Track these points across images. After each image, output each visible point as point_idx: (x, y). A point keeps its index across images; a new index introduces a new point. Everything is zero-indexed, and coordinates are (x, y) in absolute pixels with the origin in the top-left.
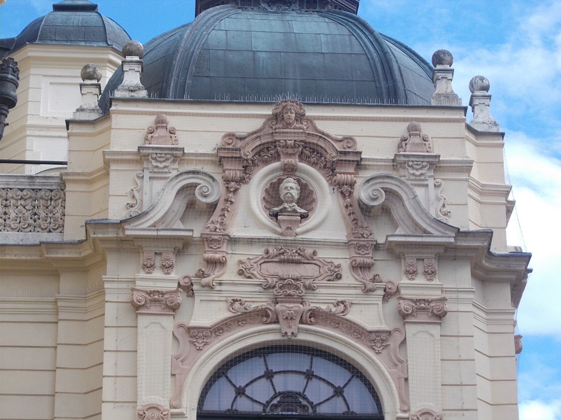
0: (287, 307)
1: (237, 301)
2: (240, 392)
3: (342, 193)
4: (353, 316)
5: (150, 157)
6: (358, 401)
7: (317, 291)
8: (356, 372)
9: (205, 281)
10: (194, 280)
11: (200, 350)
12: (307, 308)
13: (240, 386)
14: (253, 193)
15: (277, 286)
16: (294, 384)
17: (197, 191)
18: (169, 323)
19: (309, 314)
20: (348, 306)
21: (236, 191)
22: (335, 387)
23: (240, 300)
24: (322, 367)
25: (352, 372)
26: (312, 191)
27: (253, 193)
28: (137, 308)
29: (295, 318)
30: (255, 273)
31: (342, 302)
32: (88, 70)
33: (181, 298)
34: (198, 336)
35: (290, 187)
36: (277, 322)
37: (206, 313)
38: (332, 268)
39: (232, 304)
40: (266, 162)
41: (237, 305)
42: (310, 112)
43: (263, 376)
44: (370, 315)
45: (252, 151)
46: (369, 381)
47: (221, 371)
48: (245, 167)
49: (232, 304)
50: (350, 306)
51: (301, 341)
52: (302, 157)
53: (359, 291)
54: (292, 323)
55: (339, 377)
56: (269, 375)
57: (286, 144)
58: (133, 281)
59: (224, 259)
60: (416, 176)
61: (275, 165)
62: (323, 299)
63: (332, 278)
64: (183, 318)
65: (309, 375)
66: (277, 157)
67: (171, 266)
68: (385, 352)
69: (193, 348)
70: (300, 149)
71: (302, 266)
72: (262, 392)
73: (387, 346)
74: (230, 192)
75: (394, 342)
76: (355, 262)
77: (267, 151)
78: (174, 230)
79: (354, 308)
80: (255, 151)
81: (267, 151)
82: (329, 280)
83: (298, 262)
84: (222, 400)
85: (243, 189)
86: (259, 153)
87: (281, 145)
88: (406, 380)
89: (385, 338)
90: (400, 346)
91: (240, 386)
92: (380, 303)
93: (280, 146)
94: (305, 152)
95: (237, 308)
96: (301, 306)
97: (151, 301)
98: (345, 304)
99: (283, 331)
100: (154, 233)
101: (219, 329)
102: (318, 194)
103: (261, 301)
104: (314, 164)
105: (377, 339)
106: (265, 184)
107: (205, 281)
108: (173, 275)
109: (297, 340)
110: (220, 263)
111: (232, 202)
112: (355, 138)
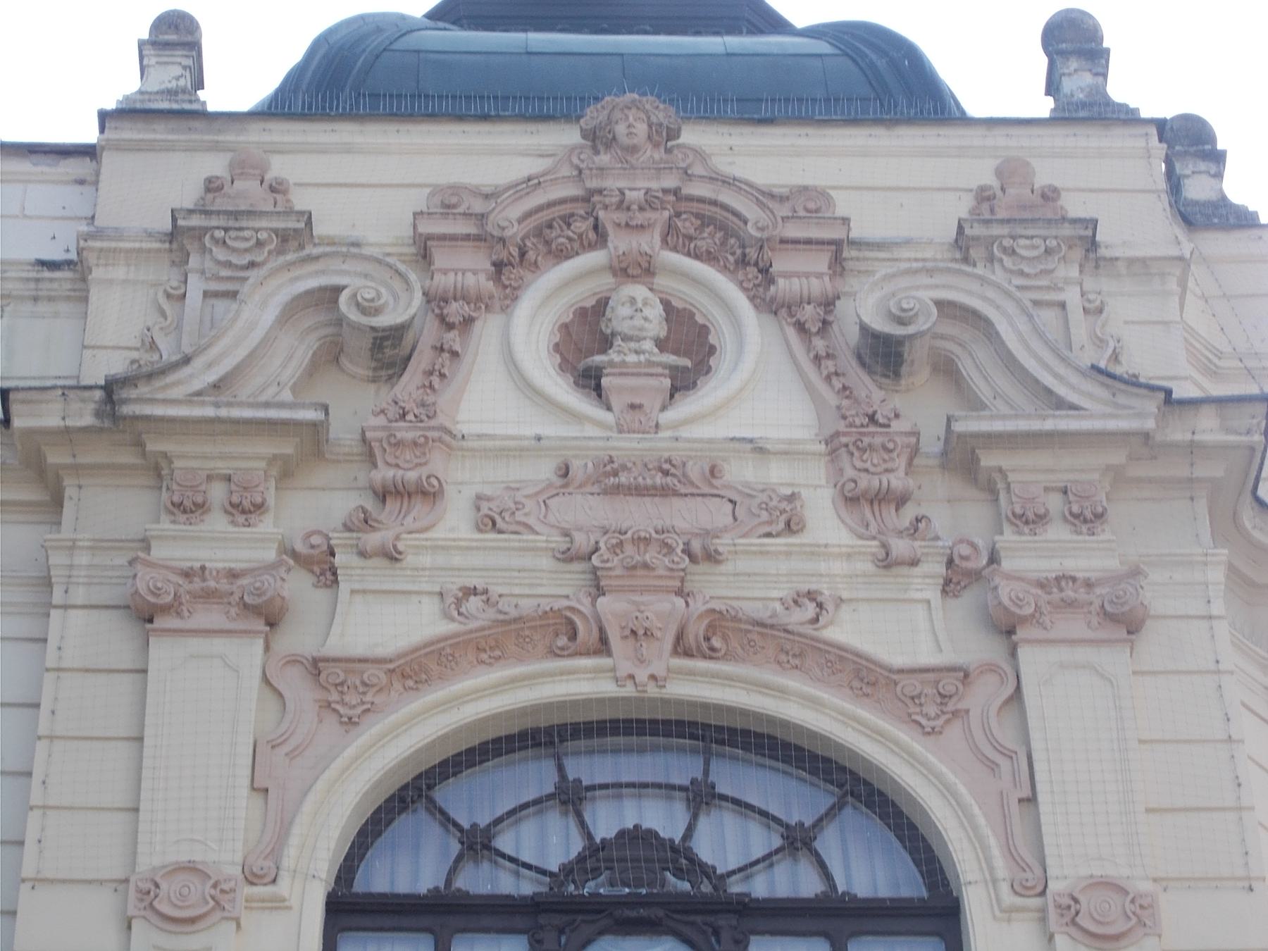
0: (634, 603)
1: (474, 591)
2: (477, 844)
3: (801, 327)
4: (843, 630)
5: (207, 239)
6: (863, 866)
7: (727, 567)
8: (858, 789)
9: (373, 540)
10: (337, 539)
11: (351, 722)
12: (698, 606)
13: (474, 826)
14: (530, 325)
15: (602, 545)
16: (664, 819)
17: (343, 298)
18: (249, 654)
19: (706, 622)
20: (830, 606)
21: (468, 322)
22: (787, 827)
23: (486, 592)
24: (733, 777)
25: (840, 786)
26: (704, 326)
27: (530, 325)
28: (145, 615)
29: (659, 634)
30: (531, 521)
31: (811, 595)
32: (177, 260)
33: (298, 587)
34: (344, 687)
35: (638, 312)
36: (603, 646)
37: (380, 620)
38: (774, 503)
39: (458, 603)
40: (562, 255)
41: (474, 603)
42: (692, 135)
43: (550, 797)
44: (906, 627)
45: (520, 221)
46: (894, 804)
47: (412, 795)
48: (499, 266)
49: (458, 603)
50: (837, 606)
51: (679, 703)
52: (672, 238)
53: (869, 567)
54: (647, 648)
55: (795, 800)
56: (571, 797)
57: (622, 202)
58: (145, 544)
59: (435, 482)
60: (1027, 276)
61: (596, 258)
62: (754, 580)
63: (774, 529)
64: (300, 638)
65: (701, 797)
66: (600, 237)
67: (259, 507)
68: (955, 731)
69: (331, 719)
70: (666, 214)
71: (677, 502)
72: (549, 844)
73: (955, 713)
74: (451, 327)
75: (983, 698)
76: (853, 485)
77: (568, 226)
78: (267, 405)
79: (845, 612)
80: (531, 223)
81: (568, 226)
82: (769, 535)
83: (665, 492)
84: (415, 866)
85: (488, 329)
86: (538, 232)
87: (607, 200)
88: (1031, 800)
89: (950, 689)
90: (1000, 708)
91: (474, 826)
92: (934, 594)
93: (606, 207)
94: (679, 224)
95: (474, 611)
96: (680, 602)
97: (195, 596)
98: (819, 599)
99: (622, 673)
100: (210, 412)
101: (415, 669)
102: (723, 335)
103: (557, 587)
104: (708, 257)
105: (931, 696)
106: (561, 310)
107: (373, 540)
108: (266, 526)
109: (666, 702)
110: (425, 493)
111: (455, 354)
112: (832, 193)
